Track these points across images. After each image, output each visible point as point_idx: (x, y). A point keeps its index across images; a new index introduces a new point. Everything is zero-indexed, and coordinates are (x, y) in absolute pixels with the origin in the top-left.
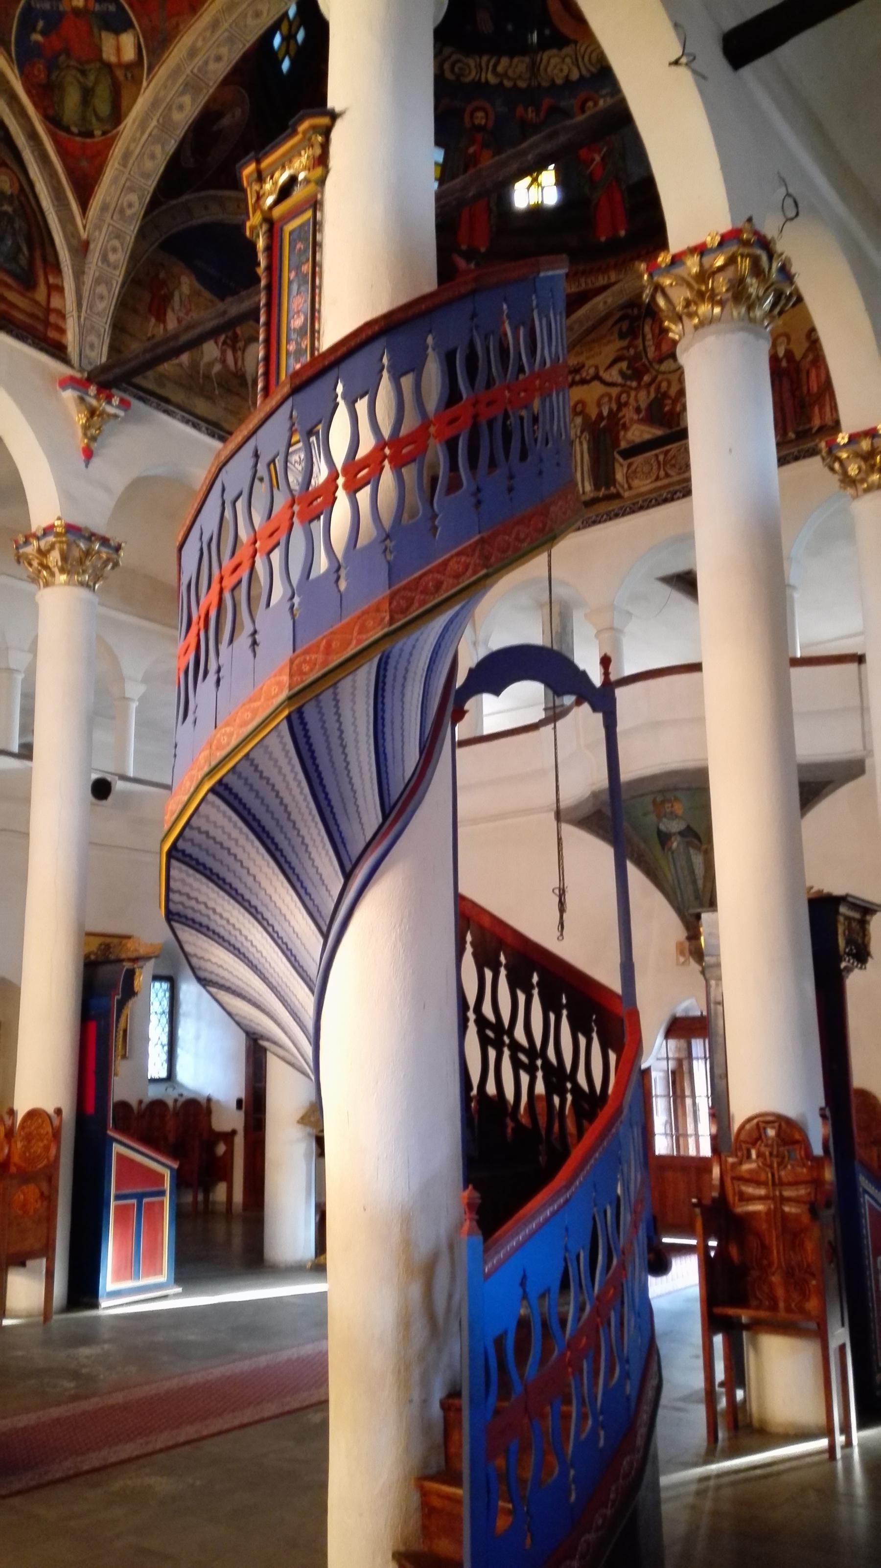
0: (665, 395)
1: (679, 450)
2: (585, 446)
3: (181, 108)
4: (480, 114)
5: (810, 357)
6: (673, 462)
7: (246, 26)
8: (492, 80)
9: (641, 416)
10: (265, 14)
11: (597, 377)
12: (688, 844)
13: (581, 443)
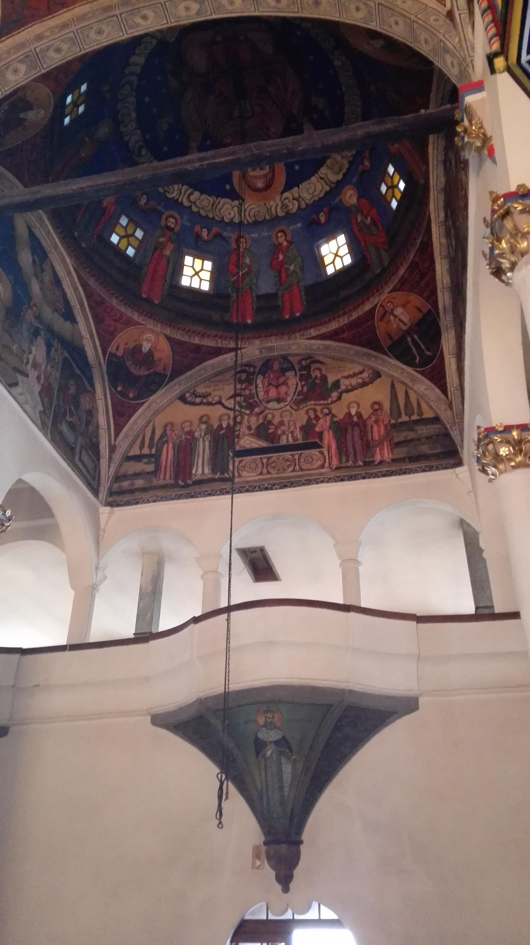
0: (270, 423)
1: (278, 459)
2: (207, 443)
3: (16, 71)
4: (172, 220)
5: (373, 418)
6: (273, 465)
7: (88, 36)
8: (186, 203)
9: (251, 432)
10: (105, 34)
11: (220, 403)
12: (281, 753)
13: (204, 441)
